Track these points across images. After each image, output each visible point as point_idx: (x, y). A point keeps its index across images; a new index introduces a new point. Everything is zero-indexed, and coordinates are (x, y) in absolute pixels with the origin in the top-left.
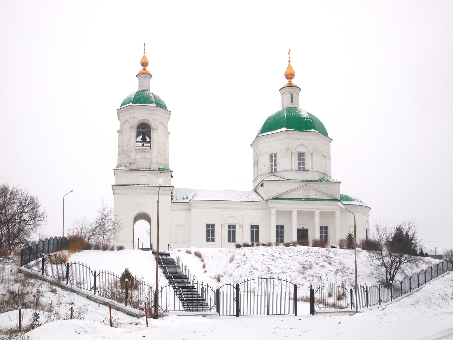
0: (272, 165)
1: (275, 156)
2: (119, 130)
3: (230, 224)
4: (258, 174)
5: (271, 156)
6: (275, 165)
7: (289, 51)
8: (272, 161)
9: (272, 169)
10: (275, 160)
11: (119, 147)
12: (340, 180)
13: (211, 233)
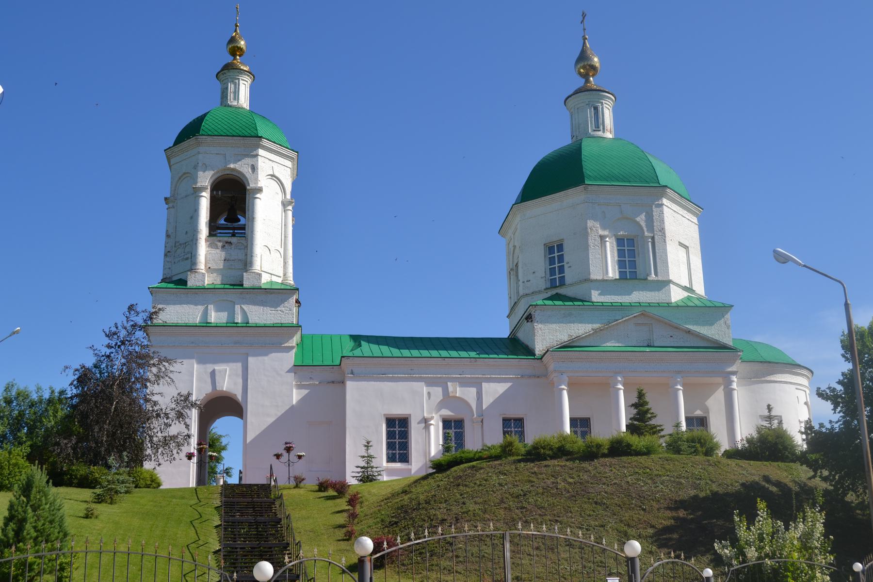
0: (552, 272)
1: (560, 247)
2: (168, 196)
3: (508, 416)
4: (518, 292)
5: (550, 249)
6: (561, 269)
7: (584, 15)
8: (552, 261)
9: (553, 281)
10: (561, 258)
11: (168, 236)
12: (728, 302)
13: (397, 441)
